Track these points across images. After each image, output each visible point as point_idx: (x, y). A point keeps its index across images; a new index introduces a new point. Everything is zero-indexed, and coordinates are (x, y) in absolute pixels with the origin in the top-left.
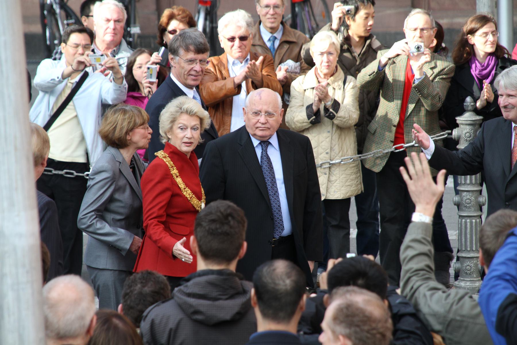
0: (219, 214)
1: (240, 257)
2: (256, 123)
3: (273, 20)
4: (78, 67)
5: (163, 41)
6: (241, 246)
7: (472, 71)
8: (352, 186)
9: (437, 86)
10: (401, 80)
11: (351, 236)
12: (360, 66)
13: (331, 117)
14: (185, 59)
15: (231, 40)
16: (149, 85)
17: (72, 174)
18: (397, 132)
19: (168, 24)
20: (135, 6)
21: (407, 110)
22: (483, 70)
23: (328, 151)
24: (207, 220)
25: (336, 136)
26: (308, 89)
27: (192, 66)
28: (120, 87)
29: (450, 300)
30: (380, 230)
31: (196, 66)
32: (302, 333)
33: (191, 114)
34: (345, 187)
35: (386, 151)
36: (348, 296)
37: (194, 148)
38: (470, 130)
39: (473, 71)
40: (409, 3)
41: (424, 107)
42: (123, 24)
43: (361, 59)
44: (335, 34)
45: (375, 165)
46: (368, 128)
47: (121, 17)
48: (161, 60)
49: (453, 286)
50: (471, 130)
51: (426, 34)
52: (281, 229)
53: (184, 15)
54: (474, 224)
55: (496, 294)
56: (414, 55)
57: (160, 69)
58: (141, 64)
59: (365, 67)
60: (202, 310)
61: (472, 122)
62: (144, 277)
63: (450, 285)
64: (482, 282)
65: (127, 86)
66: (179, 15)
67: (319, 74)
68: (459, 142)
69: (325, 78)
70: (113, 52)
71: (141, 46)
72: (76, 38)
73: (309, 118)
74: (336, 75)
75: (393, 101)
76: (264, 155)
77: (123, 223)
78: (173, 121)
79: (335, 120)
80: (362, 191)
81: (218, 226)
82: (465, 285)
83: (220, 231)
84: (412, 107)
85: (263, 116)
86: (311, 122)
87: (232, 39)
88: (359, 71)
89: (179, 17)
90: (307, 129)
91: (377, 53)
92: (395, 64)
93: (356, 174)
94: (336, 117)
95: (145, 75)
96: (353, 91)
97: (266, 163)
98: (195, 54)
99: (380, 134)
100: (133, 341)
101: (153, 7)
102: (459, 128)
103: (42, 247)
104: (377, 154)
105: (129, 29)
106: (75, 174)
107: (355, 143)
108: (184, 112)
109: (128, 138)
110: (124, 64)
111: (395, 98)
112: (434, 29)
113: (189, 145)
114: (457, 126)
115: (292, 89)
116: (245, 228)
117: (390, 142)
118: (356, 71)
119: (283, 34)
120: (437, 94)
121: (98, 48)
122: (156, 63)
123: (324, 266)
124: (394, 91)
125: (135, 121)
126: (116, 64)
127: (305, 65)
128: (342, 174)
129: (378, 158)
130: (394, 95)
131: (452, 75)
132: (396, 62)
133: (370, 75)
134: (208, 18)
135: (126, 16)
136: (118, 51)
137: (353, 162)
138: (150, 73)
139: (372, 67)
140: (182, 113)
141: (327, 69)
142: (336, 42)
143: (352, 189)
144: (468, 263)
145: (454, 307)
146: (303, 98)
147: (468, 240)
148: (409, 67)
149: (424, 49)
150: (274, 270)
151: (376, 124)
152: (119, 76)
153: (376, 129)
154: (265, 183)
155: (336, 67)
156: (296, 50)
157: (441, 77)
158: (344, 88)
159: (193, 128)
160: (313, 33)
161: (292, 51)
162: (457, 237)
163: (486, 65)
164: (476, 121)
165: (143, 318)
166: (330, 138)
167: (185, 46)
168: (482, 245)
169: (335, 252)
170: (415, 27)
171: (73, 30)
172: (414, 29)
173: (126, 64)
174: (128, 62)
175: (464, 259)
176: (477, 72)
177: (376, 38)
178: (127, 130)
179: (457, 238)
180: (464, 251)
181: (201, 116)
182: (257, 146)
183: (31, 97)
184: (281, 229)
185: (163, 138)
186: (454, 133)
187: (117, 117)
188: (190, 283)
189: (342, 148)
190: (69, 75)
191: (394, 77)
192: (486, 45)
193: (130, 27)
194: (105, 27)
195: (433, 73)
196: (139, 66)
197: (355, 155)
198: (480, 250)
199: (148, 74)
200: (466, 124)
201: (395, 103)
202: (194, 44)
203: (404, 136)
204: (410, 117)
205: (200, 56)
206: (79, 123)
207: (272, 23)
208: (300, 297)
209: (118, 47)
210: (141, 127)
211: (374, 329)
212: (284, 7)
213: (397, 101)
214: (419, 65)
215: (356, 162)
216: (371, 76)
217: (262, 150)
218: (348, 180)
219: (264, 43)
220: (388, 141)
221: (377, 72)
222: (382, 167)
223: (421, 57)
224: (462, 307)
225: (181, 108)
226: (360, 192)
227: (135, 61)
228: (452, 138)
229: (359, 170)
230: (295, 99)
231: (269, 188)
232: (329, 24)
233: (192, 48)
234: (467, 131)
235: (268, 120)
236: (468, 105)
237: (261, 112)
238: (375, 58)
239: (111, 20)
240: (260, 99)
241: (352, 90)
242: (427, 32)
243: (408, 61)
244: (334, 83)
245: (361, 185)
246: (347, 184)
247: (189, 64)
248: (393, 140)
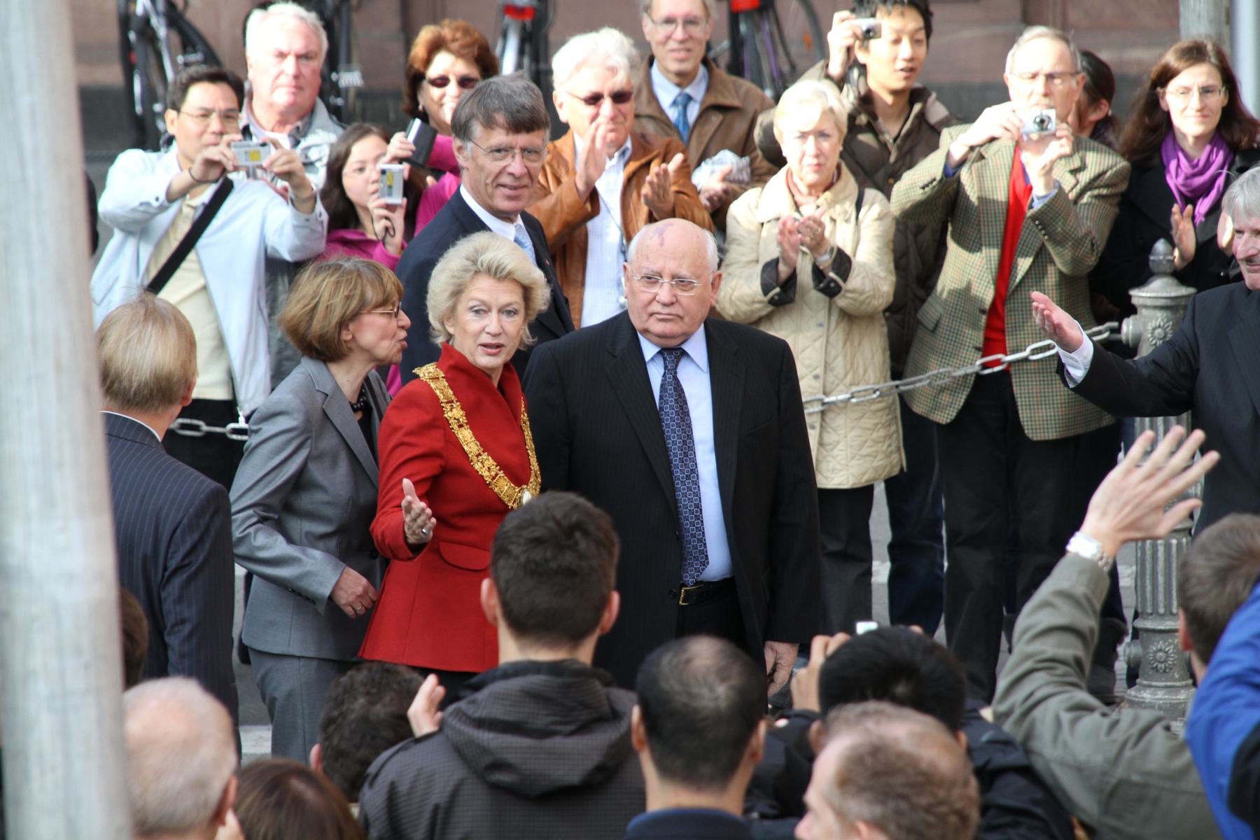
0: (551, 524)
1: (602, 629)
2: (650, 302)
3: (682, 54)
4: (205, 173)
5: (417, 104)
6: (605, 602)
7: (1168, 178)
8: (875, 457)
9: (1085, 215)
10: (999, 200)
11: (873, 579)
12: (898, 165)
13: (831, 291)
14: (485, 146)
16: (385, 212)
17: (196, 428)
18: (989, 327)
19: (428, 61)
21: (1012, 273)
23: (820, 371)
24: (522, 541)
25: (838, 336)
27: (502, 164)
28: (308, 220)
29: (1119, 735)
30: (946, 564)
31: (513, 164)
32: (755, 815)
33: (498, 276)
34: (859, 459)
35: (961, 372)
36: (870, 724)
37: (509, 358)
38: (1165, 320)
39: (1172, 178)
40: (1016, 11)
41: (1055, 265)
42: (318, 63)
43: (899, 148)
44: (836, 90)
45: (936, 407)
46: (919, 316)
47: (313, 48)
48: (413, 151)
49: (1123, 699)
50: (1167, 322)
51: (1060, 87)
52: (701, 562)
53: (468, 40)
54: (1174, 550)
55: (1228, 719)
56: (1030, 139)
57: (411, 172)
58: (364, 162)
59: (910, 167)
60: (513, 761)
61: (1169, 303)
62: (373, 680)
63: (1117, 697)
64: (1193, 690)
65: (325, 217)
66: (454, 40)
67: (795, 185)
68: (1139, 350)
69: (810, 194)
70: (295, 131)
71: (364, 119)
72: (202, 95)
73: (766, 292)
74: (838, 186)
75: (980, 250)
76: (668, 382)
77: (332, 543)
78: (457, 293)
79: (840, 298)
80: (902, 469)
81: (549, 555)
82: (1152, 697)
83: (553, 565)
84: (1024, 266)
85: (666, 287)
86: (771, 302)
87: (595, 99)
88: (896, 176)
89: (455, 46)
90: (769, 317)
91: (939, 134)
92: (983, 161)
93: (888, 428)
94: (842, 292)
95: (372, 188)
96: (879, 226)
97: (671, 401)
98: (508, 134)
99: (950, 331)
100: (340, 832)
101: (392, 22)
102: (1138, 316)
103: (124, 604)
104: (940, 378)
105: (334, 76)
106: (205, 428)
107: (884, 351)
108: (482, 270)
109: (346, 336)
110: (320, 159)
111: (983, 243)
112: (1079, 77)
113: (494, 351)
114: (1131, 310)
115: (729, 220)
116: (616, 560)
117: (973, 350)
118: (888, 179)
119: (709, 88)
120: (1085, 234)
121: (258, 122)
122: (401, 160)
123: (805, 652)
124: (982, 227)
125: (363, 294)
126: (297, 165)
127: (765, 165)
128: (853, 428)
129: (945, 388)
130: (983, 235)
131: (1123, 187)
132: (986, 156)
133: (923, 188)
134: (528, 48)
135: (325, 45)
136: (305, 129)
137: (880, 399)
138: (388, 183)
139: (928, 169)
140: (477, 272)
141: (816, 172)
142: (836, 106)
143: (876, 464)
144: (1161, 645)
145: (1128, 753)
146: (758, 244)
147: (1161, 589)
148: (1017, 165)
149: (1057, 124)
150: (688, 661)
151: (938, 306)
152: (306, 194)
153: (940, 319)
154: (666, 451)
155: (839, 168)
156: (740, 127)
157: (1096, 192)
158: (857, 218)
159: (506, 311)
160: (782, 84)
162: (1133, 581)
164: (1179, 300)
165: (369, 779)
166: (824, 339)
167: (483, 116)
168: (1185, 603)
169: (835, 617)
170: (1034, 70)
171: (195, 75)
172: (1030, 76)
173: (325, 160)
174: (330, 156)
175: (1150, 634)
176: (1181, 180)
177: (938, 99)
178: (342, 317)
179: (1134, 585)
180: (1151, 614)
181: (526, 282)
182: (652, 359)
183: (95, 242)
184: (701, 562)
185: (437, 333)
186: (1125, 328)
187: (319, 286)
188: (481, 695)
189: (852, 364)
190: (183, 193)
191: (981, 191)
192: (1185, 117)
193: (337, 72)
194: (274, 72)
195: (1078, 182)
196: (357, 166)
197: (885, 381)
198: (1182, 616)
199: (382, 185)
200: (1156, 307)
201: (984, 255)
202: (506, 110)
203: (1005, 336)
204: (1019, 289)
205: (522, 139)
206: (211, 304)
207: (682, 61)
208: (751, 727)
209: (306, 119)
210: (380, 310)
211: (942, 803)
212: (710, 20)
213: (988, 250)
214: (1042, 165)
215: (886, 398)
216: (927, 189)
217: (665, 369)
218: (866, 442)
219: (662, 111)
220: (969, 347)
221: (941, 180)
222: (956, 411)
223: (1049, 143)
224: (1146, 751)
225: (474, 262)
226: (896, 472)
227: (347, 154)
228: (1120, 341)
229: (896, 417)
230: (739, 244)
231: (676, 461)
232: (821, 63)
233: (500, 118)
234: (1157, 324)
235: (679, 298)
236: (1160, 261)
237: (661, 277)
238: (934, 147)
239: (289, 54)
240: (662, 244)
241: (877, 223)
242: (1061, 84)
243: (1015, 151)
244: (834, 206)
245: (900, 454)
246: (865, 451)
247: (496, 160)
248: (981, 346)
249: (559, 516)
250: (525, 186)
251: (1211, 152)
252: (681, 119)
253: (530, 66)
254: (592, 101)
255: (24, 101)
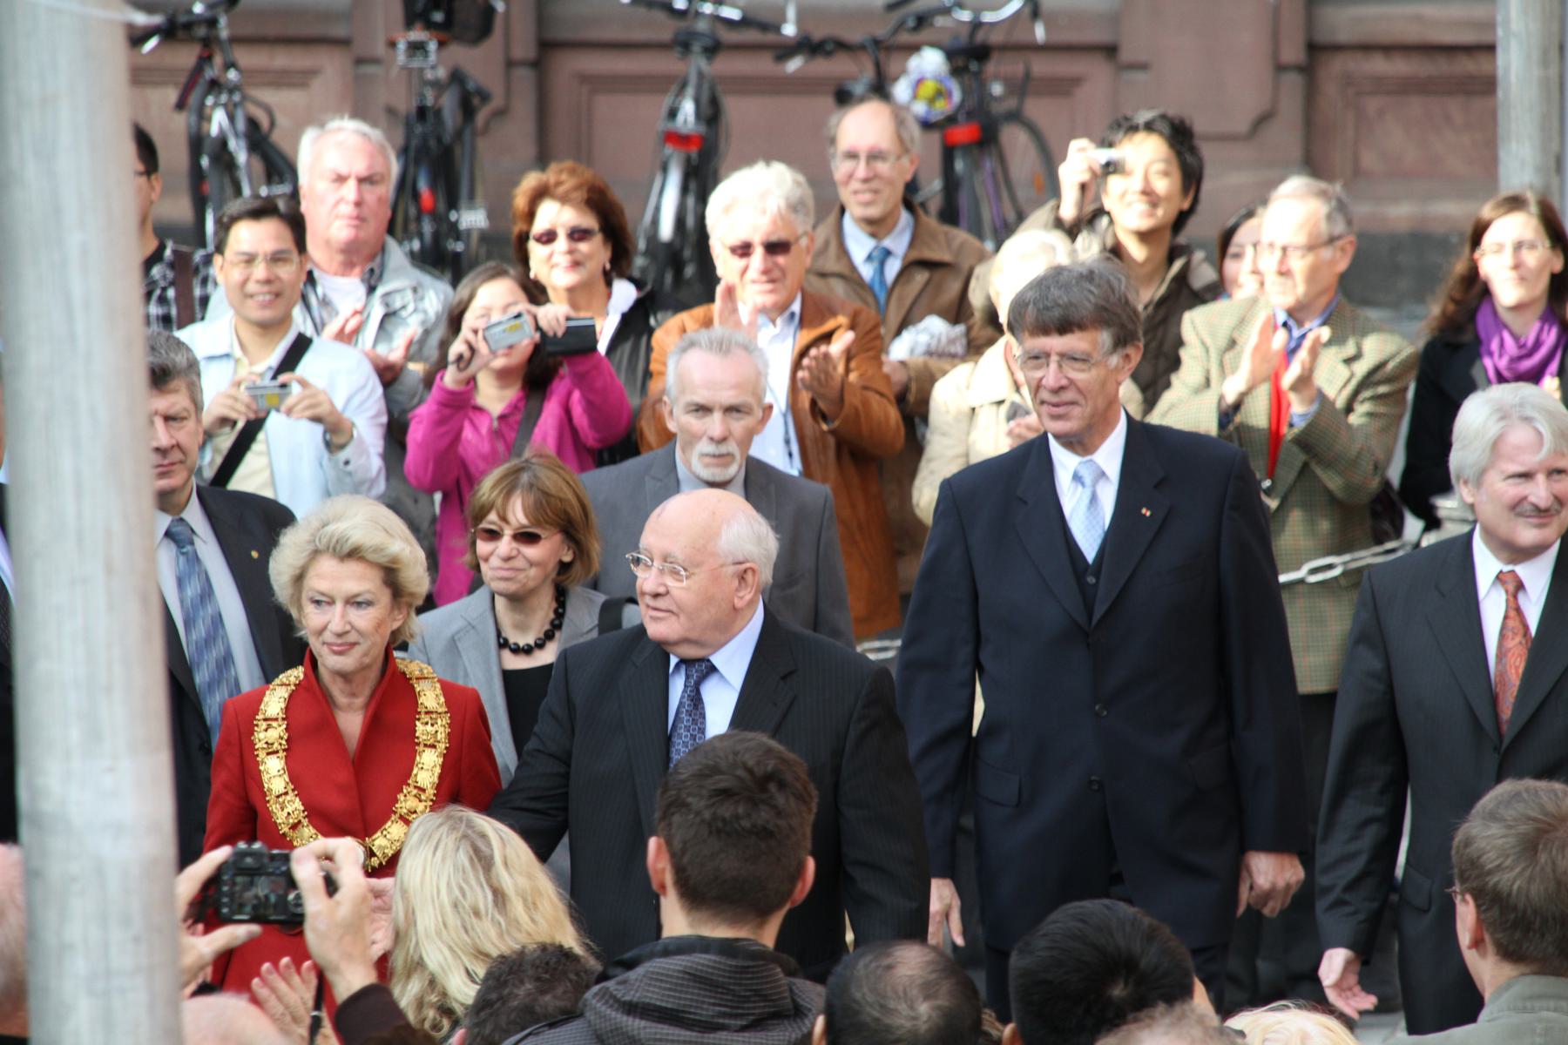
0: (740, 772)
3: (867, 197)
6: (801, 867)
15: (1272, 321)
20: (473, 148)
22: (1520, 358)
24: (704, 792)
26: (982, 406)
81: (741, 810)
83: (746, 824)
87: (744, 250)
105: (453, 216)
134: (693, 186)
156: (954, 288)
160: (1004, 231)
161: (939, 289)
163: (1530, 342)
188: (632, 975)
194: (331, 199)
207: (867, 204)
219: (853, 268)
249: (751, 763)
250: (1073, 403)
251: (1541, 330)
252: (877, 279)
253: (695, 208)
254: (740, 251)
255: (74, 239)
